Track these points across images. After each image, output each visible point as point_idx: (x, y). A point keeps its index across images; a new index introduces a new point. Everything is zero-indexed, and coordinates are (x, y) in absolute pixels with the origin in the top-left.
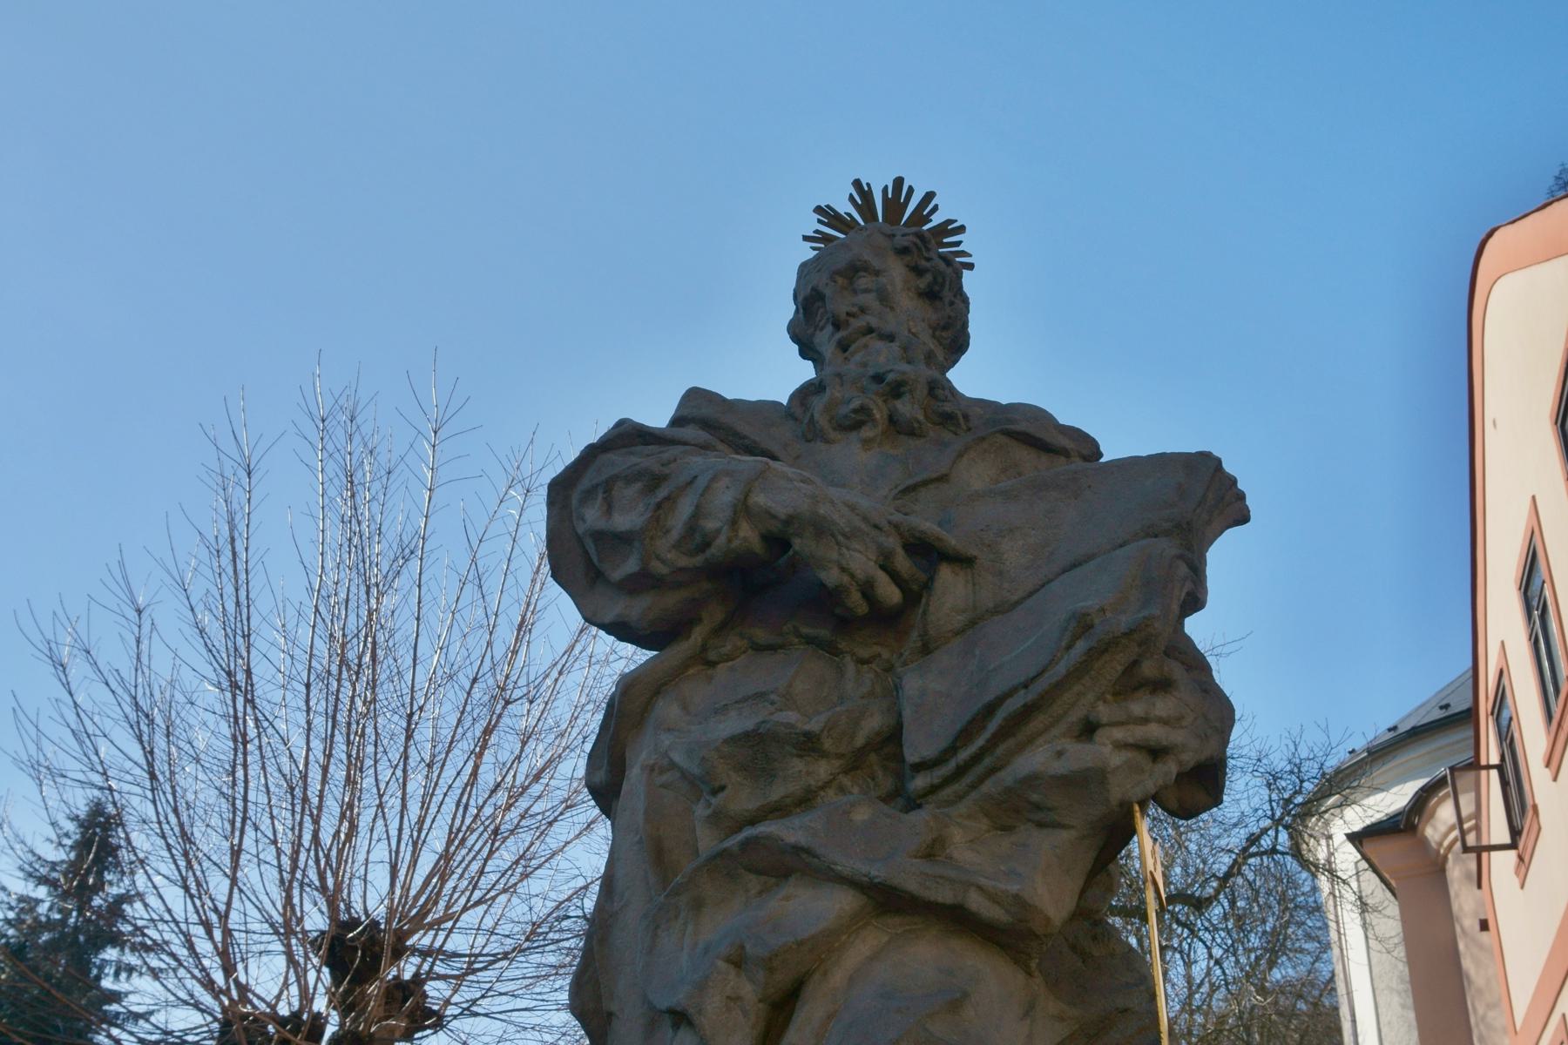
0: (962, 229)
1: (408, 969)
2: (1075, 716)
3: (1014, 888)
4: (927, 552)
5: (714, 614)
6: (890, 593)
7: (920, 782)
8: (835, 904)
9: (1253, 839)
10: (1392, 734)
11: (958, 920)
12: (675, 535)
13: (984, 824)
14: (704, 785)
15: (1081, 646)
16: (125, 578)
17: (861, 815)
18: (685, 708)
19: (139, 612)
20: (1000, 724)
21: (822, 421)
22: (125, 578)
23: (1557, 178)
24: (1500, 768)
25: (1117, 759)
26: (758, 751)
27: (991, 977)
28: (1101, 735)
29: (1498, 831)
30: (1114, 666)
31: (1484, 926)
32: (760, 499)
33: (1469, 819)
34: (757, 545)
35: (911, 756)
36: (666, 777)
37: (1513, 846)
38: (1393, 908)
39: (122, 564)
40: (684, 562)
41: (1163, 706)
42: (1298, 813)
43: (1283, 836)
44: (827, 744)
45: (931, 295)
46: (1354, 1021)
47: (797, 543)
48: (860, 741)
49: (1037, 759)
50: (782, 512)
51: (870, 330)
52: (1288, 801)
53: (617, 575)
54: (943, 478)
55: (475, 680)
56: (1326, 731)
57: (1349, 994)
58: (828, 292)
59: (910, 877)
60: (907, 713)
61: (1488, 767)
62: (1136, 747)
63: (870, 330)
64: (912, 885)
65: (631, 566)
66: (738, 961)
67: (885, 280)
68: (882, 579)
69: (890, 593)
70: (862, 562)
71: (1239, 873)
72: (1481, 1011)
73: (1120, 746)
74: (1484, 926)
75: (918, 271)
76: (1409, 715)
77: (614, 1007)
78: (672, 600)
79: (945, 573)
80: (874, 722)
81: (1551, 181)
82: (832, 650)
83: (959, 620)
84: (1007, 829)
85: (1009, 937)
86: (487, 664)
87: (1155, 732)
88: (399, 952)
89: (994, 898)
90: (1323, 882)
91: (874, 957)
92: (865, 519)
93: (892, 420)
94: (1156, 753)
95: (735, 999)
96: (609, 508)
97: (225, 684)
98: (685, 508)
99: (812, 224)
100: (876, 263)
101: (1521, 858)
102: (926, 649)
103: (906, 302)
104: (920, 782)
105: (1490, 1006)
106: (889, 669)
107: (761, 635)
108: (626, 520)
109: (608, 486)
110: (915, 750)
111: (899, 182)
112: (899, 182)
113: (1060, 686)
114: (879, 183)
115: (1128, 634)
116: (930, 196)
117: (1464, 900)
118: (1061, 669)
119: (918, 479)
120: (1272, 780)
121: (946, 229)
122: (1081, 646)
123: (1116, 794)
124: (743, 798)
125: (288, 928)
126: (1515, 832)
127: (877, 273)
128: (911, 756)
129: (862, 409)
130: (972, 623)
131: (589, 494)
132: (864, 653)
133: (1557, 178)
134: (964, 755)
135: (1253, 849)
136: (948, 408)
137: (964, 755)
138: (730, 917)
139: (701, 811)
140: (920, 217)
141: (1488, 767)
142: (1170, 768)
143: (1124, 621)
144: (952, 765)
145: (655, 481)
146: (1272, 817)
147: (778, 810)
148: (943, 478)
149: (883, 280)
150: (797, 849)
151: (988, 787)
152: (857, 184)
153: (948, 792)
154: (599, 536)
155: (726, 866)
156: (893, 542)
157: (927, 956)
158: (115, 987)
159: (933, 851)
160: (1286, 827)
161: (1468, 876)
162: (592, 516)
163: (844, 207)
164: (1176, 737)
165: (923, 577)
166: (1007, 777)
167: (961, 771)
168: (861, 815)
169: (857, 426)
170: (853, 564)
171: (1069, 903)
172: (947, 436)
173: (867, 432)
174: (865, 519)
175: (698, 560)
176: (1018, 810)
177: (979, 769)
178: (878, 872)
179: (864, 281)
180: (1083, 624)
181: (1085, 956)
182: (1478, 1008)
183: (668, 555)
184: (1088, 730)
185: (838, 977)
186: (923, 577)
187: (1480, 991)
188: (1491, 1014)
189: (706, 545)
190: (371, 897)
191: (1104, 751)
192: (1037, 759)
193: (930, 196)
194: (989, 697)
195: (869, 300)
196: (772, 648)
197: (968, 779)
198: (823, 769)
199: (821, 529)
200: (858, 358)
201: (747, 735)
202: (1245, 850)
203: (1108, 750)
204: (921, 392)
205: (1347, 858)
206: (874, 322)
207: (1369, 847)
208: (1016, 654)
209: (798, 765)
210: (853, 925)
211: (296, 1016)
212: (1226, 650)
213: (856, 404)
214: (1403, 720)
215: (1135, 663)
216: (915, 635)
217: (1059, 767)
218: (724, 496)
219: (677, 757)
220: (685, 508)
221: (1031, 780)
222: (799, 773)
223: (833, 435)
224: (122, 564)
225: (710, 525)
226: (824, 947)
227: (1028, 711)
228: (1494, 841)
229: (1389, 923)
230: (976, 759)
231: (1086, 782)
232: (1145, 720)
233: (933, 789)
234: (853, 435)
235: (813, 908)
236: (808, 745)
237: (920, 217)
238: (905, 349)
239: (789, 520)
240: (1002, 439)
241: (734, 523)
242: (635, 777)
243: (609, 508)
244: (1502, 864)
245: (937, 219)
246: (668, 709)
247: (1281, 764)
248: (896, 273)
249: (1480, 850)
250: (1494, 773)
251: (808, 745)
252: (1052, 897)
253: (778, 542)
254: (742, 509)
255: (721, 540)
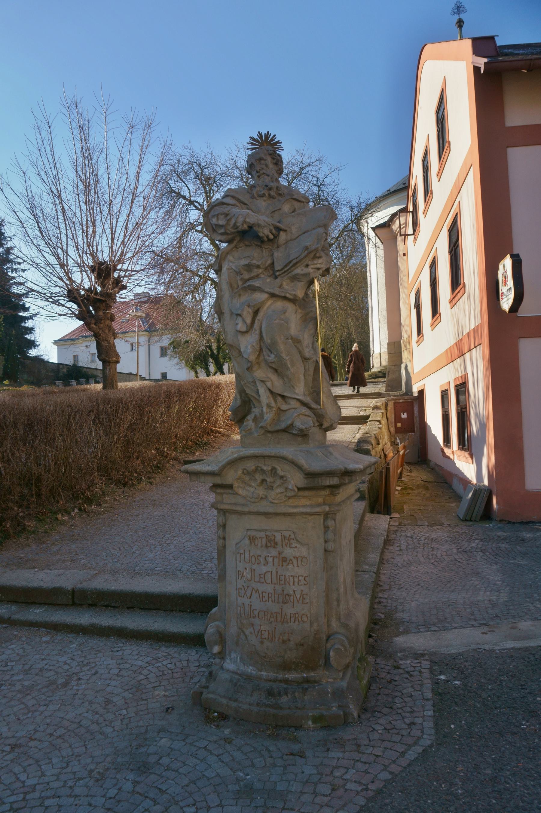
0: (281, 143)
1: (116, 275)
2: (305, 264)
3: (294, 293)
4: (279, 229)
5: (238, 239)
6: (271, 237)
7: (278, 273)
8: (265, 296)
9: (346, 227)
10: (388, 192)
11: (285, 298)
12: (231, 226)
13: (289, 281)
14: (238, 273)
15: (306, 252)
16: (18, 163)
17: (268, 280)
18: (233, 257)
19: (24, 173)
20: (291, 265)
21: (256, 195)
22: (18, 163)
23: (455, 4)
24: (412, 212)
25: (312, 271)
26: (249, 267)
27: (290, 307)
28: (309, 267)
29: (410, 231)
30: (312, 255)
31: (404, 255)
32: (248, 220)
33: (403, 224)
34: (247, 228)
35: (276, 269)
36: (231, 271)
37: (413, 234)
38: (382, 247)
39: (16, 158)
40: (233, 231)
41: (320, 261)
42: (359, 216)
43: (354, 226)
44: (261, 266)
45: (276, 164)
46: (371, 277)
47: (255, 228)
48: (267, 265)
49: (299, 271)
50: (252, 223)
51: (264, 174)
52: (356, 215)
53: (220, 232)
54: (280, 209)
55: (124, 190)
56: (368, 194)
57: (370, 270)
58: (255, 164)
59: (277, 291)
60: (275, 260)
61: (410, 212)
62: (315, 268)
63: (264, 174)
64: (277, 293)
65: (222, 231)
66: (249, 306)
67: (265, 152)
68: (270, 234)
69: (271, 237)
70: (266, 232)
71: (341, 236)
72: (402, 276)
73: (312, 268)
74: (404, 255)
75: (273, 159)
76: (394, 186)
77: (224, 311)
78: (230, 237)
79: (281, 233)
80: (269, 262)
81: (454, 6)
82: (261, 247)
83: (284, 242)
84: (293, 281)
85: (293, 301)
86: (128, 185)
87: (318, 266)
88: (115, 270)
89: (291, 295)
90: (366, 240)
91: (271, 304)
92: (267, 223)
93: (269, 195)
94: (318, 269)
95: (248, 312)
96: (218, 219)
97: (50, 192)
98: (233, 221)
99: (249, 140)
100: (265, 158)
101: (415, 238)
102: (278, 247)
103: (271, 166)
104: (278, 273)
105: (404, 276)
106: (271, 250)
107: (247, 243)
108: (222, 222)
109: (218, 215)
110: (277, 267)
111: (268, 132)
112: (268, 132)
113: (302, 259)
114: (264, 133)
115: (315, 250)
116: (275, 135)
117: (401, 246)
118: (303, 256)
119: (275, 209)
120: (352, 208)
121: (278, 142)
122: (306, 252)
123: (311, 277)
124: (246, 276)
125: (81, 266)
126: (414, 230)
127: (265, 160)
128: (276, 269)
129: (264, 194)
130: (286, 243)
131: (213, 216)
132: (266, 247)
133: (455, 4)
134: (286, 269)
135: (346, 230)
136: (280, 192)
137: (286, 269)
138: (245, 298)
139: (238, 278)
140: (272, 139)
141: (410, 212)
142: (321, 271)
143: (313, 248)
144: (284, 271)
145: (227, 215)
146: (351, 220)
147: (253, 278)
148: (280, 209)
149: (266, 162)
150: (258, 287)
151: (290, 275)
152: (259, 132)
153: (282, 275)
154: (216, 225)
155: (245, 289)
156: (272, 228)
157: (279, 304)
158: (12, 275)
159: (280, 287)
160: (355, 223)
161: (402, 240)
162: (214, 221)
163: (256, 137)
164: (322, 266)
165: (277, 233)
166: (293, 273)
167: (285, 272)
168: (268, 280)
169: (263, 197)
170: (265, 232)
171: (303, 294)
172: (280, 198)
173: (265, 198)
174: (267, 223)
175: (236, 230)
176: (295, 278)
177: (288, 272)
178: (272, 291)
179: (262, 162)
180: (306, 248)
181: (305, 301)
182: (401, 275)
183: (230, 229)
184: (307, 266)
185: (265, 308)
186: (277, 233)
187: (402, 272)
188: (404, 278)
189: (237, 228)
190: (105, 255)
191: (310, 270)
192: (299, 271)
193: (275, 135)
194: (291, 260)
195: (264, 166)
196: (250, 246)
197: (286, 273)
198: (260, 271)
199: (259, 225)
200: (262, 179)
201: (247, 265)
202: (343, 229)
203: (310, 269)
204: (275, 190)
205: (372, 234)
206: (265, 172)
207: (377, 231)
208: (295, 252)
209: (256, 270)
210: (267, 299)
211: (90, 288)
212: (341, 168)
213: (262, 192)
214: (392, 187)
215: (316, 254)
216: (276, 244)
217: (302, 272)
218: (241, 219)
219: (233, 268)
220: (233, 221)
221: (297, 274)
222: (256, 271)
223: (258, 198)
224: (16, 158)
225: (238, 224)
226: (263, 303)
227: (297, 263)
228: (409, 233)
229: (381, 252)
230: (288, 270)
231: (306, 275)
232: (317, 264)
233: (280, 275)
234: (262, 198)
235: (260, 297)
236: (258, 267)
237: (272, 139)
238: (271, 178)
239: (253, 224)
240: (291, 200)
241: (243, 224)
242: (224, 269)
243: (218, 219)
244: (410, 239)
245: (276, 140)
246: (230, 257)
247: (355, 204)
248: (269, 159)
249: (406, 235)
250: (411, 213)
251: (258, 267)
252: (300, 294)
253: (250, 227)
254: (245, 222)
255: (240, 227)
